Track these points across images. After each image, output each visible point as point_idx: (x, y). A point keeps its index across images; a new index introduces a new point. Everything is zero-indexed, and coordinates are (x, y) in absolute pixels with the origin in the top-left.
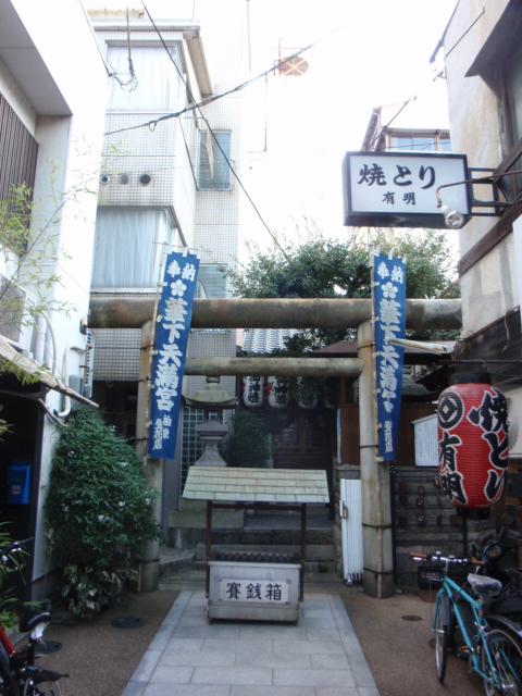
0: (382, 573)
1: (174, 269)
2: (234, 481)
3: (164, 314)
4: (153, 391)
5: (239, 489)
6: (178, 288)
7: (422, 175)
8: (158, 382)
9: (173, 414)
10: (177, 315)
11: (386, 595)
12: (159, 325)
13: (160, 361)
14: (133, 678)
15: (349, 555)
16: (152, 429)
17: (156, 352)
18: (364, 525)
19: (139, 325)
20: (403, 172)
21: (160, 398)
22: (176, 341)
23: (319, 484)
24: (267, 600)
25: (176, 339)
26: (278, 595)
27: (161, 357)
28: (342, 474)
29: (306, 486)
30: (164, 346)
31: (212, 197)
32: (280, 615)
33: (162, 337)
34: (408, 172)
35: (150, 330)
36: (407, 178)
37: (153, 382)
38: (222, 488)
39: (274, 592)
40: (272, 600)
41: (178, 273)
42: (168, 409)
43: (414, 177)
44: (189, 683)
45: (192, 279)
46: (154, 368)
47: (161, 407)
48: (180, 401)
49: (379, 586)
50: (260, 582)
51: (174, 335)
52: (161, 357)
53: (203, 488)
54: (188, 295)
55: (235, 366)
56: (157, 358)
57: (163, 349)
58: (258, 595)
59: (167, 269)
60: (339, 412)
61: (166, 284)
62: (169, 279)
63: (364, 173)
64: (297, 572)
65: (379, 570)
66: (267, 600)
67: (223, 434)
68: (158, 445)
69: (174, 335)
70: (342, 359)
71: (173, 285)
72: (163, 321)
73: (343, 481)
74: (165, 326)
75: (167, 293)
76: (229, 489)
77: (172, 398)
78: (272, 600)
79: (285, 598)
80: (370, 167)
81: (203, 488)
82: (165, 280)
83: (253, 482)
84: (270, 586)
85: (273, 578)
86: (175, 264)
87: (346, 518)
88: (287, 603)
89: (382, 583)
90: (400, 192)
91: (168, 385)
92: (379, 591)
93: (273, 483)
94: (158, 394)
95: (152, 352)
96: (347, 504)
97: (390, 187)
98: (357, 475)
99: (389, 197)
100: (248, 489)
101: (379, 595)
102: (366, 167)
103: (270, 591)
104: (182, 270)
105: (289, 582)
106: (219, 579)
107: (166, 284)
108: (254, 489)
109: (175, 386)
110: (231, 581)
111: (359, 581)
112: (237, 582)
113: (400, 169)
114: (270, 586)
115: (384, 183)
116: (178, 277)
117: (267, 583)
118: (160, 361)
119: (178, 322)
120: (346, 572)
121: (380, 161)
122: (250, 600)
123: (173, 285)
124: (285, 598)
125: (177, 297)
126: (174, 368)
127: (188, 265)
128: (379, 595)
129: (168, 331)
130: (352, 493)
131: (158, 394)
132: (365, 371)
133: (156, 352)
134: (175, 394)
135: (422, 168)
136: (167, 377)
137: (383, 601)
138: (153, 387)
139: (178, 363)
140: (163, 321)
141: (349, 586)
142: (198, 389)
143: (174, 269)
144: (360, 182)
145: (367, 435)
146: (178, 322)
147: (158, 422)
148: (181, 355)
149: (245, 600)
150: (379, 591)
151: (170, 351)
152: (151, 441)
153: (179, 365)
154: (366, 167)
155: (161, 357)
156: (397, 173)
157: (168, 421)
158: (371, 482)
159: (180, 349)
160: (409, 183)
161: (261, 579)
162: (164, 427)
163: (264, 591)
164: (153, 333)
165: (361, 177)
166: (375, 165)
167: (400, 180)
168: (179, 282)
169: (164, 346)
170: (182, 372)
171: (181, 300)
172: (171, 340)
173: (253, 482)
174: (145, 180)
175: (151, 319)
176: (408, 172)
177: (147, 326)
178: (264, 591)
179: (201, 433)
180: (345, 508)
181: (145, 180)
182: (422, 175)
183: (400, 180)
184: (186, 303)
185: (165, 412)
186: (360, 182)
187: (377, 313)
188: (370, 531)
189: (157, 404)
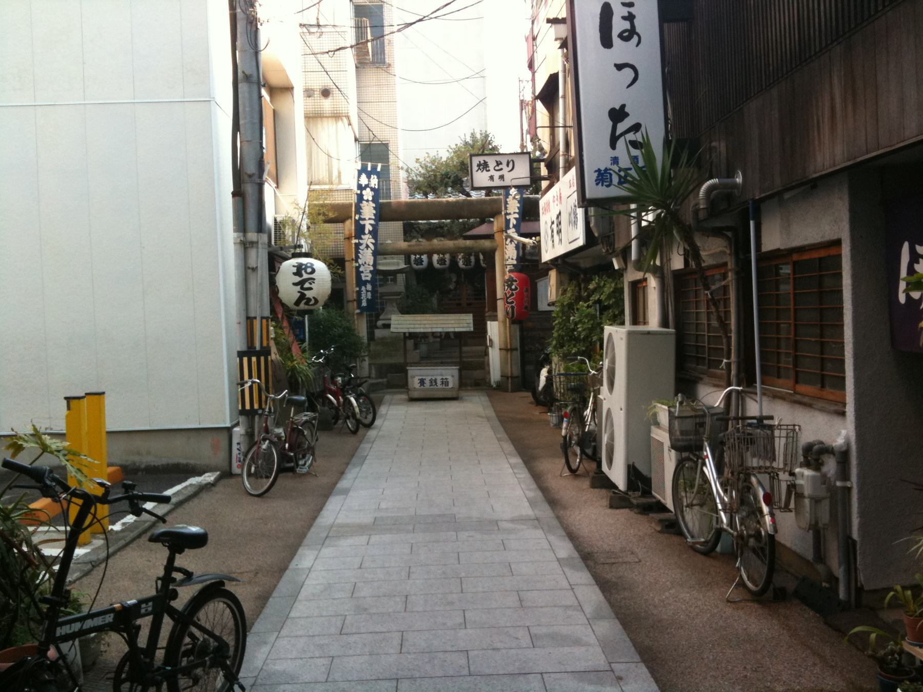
0: (512, 377)
1: (364, 180)
2: (419, 322)
3: (360, 214)
4: (358, 268)
5: (422, 326)
6: (368, 194)
7: (508, 165)
8: (360, 261)
9: (372, 282)
10: (368, 211)
11: (513, 391)
12: (357, 222)
13: (361, 247)
14: (293, 565)
15: (494, 370)
16: (359, 293)
17: (357, 241)
18: (500, 349)
19: (343, 221)
20: (498, 163)
21: (362, 272)
22: (514, 226)
23: (468, 321)
24: (441, 387)
25: (369, 231)
26: (447, 384)
27: (361, 244)
28: (487, 318)
29: (462, 323)
30: (363, 236)
31: (372, 75)
32: (449, 395)
33: (360, 230)
34: (501, 163)
35: (350, 226)
36: (500, 167)
37: (357, 261)
38: (412, 326)
39: (445, 382)
40: (444, 387)
41: (367, 183)
42: (369, 279)
43: (504, 166)
44: (326, 682)
45: (377, 187)
46: (357, 252)
47: (364, 279)
48: (375, 272)
49: (510, 385)
50: (436, 377)
51: (368, 228)
52: (361, 244)
53: (401, 326)
54: (375, 200)
55: (412, 248)
56: (358, 246)
57: (362, 239)
58: (436, 384)
59: (358, 181)
60: (293, 409)
61: (359, 192)
62: (360, 187)
63: (479, 165)
64: (457, 371)
65: (509, 375)
66: (441, 387)
67: (399, 294)
68: (364, 304)
69: (368, 228)
70: (483, 241)
71: (364, 192)
72: (360, 219)
73: (489, 323)
74: (362, 223)
75: (360, 198)
76: (417, 326)
77: (371, 272)
78: (444, 387)
79: (451, 385)
80: (482, 162)
81: (401, 326)
82: (358, 189)
83: (430, 322)
84: (442, 379)
85: (449, 375)
86: (364, 176)
87: (491, 346)
88: (452, 388)
89: (511, 383)
90: (497, 175)
91: (511, 258)
92: (510, 388)
93: (442, 322)
94: (361, 269)
95: (354, 241)
96: (492, 338)
97: (492, 172)
98: (494, 318)
99: (492, 178)
100: (427, 326)
101: (510, 391)
102: (480, 162)
103: (442, 382)
104: (369, 181)
105: (453, 376)
106: (413, 377)
107: (359, 192)
108: (430, 326)
109: (371, 263)
110: (420, 378)
111: (501, 387)
112: (424, 378)
113: (497, 162)
114: (442, 379)
115: (489, 170)
116: (367, 186)
117: (441, 377)
118: (361, 247)
119: (370, 219)
120: (492, 381)
121: (487, 159)
122: (432, 387)
123: (364, 192)
124: (451, 385)
125: (367, 201)
126: (369, 252)
127: (372, 176)
128: (510, 391)
129: (364, 225)
130: (494, 330)
131: (361, 269)
132: (498, 249)
133: (357, 241)
134: (372, 268)
135: (508, 161)
136: (367, 257)
137: (511, 394)
138: (357, 265)
139: (372, 247)
140: (360, 219)
141: (495, 389)
142: (387, 265)
143: (364, 180)
144: (477, 171)
145: (500, 293)
146: (370, 219)
147: (363, 288)
148: (373, 241)
149: (429, 387)
150: (510, 388)
151: (367, 239)
152: (359, 301)
153: (373, 249)
154: (480, 162)
155: (360, 244)
156: (496, 164)
157: (369, 287)
158: (505, 322)
159: (373, 238)
160: (501, 169)
161: (437, 375)
162: (367, 291)
163: (439, 382)
164: (353, 228)
165: (477, 168)
166: (484, 161)
167: (497, 168)
168: (368, 189)
169: (363, 236)
170: (376, 253)
171: (371, 203)
172: (367, 231)
173: (430, 322)
174: (326, 93)
175: (351, 217)
176: (501, 163)
177: (348, 222)
178: (439, 382)
179: (383, 295)
180: (491, 340)
181: (326, 93)
182: (508, 165)
183: (497, 168)
184: (374, 205)
185: (367, 281)
186: (477, 171)
187: (506, 208)
188: (503, 351)
189: (361, 277)
